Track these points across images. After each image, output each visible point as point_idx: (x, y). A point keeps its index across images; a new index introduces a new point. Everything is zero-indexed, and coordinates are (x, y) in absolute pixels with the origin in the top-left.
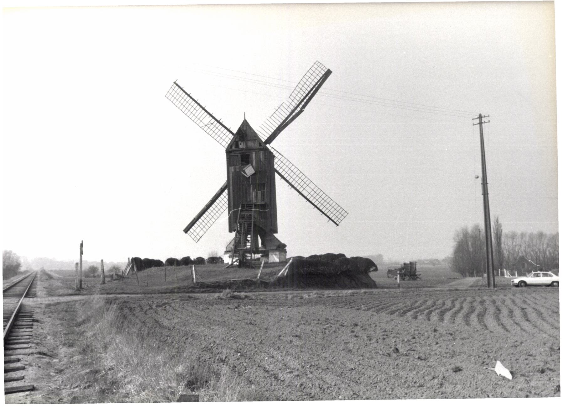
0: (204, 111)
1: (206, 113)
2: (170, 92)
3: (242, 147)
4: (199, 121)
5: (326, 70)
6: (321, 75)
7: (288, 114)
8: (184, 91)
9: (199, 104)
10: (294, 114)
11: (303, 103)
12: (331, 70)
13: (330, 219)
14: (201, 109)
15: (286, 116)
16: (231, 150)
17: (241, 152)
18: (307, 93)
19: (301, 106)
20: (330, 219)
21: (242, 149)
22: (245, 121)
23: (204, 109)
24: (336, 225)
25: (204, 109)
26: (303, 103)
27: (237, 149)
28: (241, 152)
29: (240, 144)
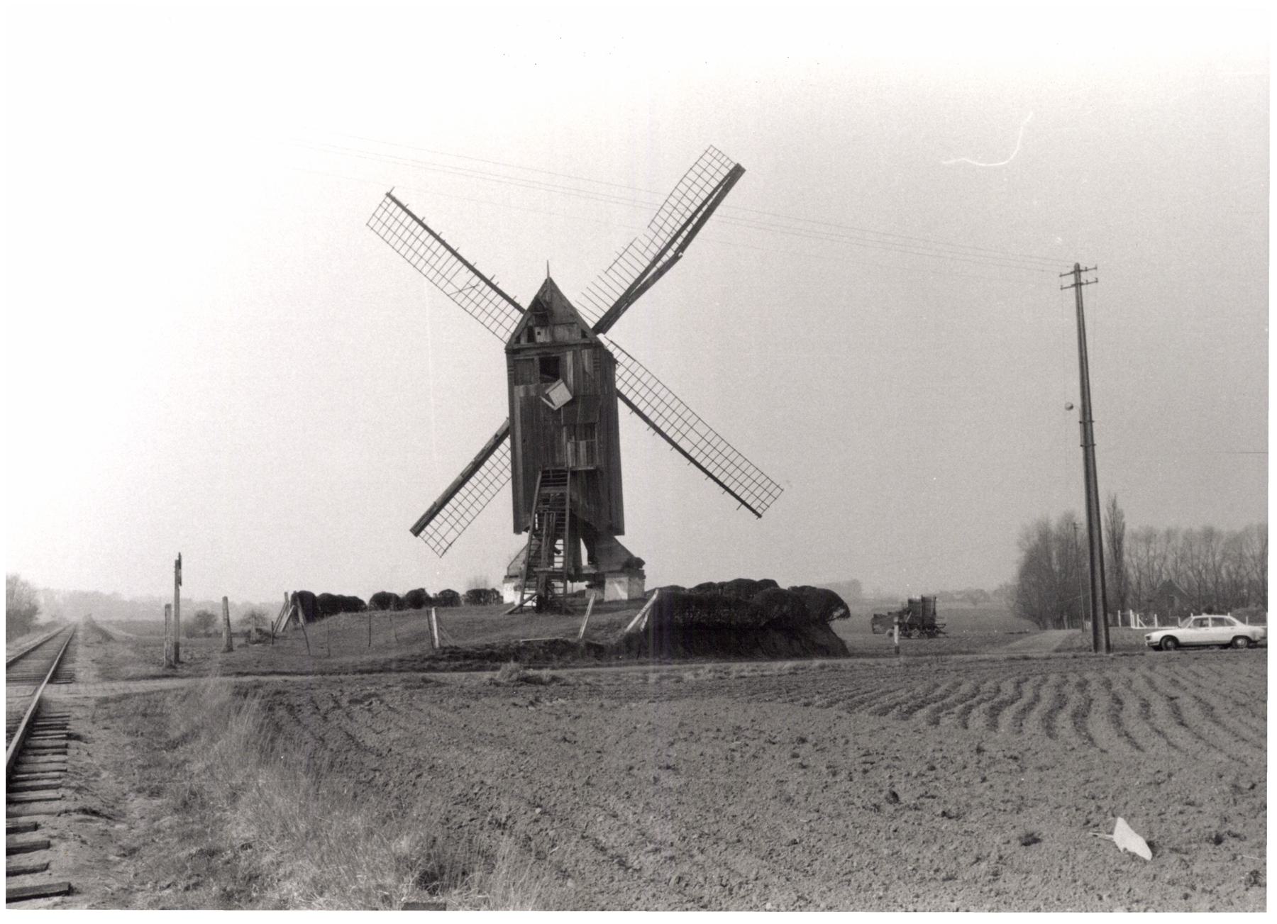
0: (454, 259)
1: (460, 264)
2: (378, 215)
3: (542, 341)
4: (444, 281)
5: (731, 167)
6: (720, 178)
7: (647, 263)
8: (409, 213)
9: (443, 243)
10: (659, 264)
11: (680, 240)
12: (743, 165)
13: (743, 502)
14: (448, 253)
15: (642, 269)
16: (516, 347)
17: (539, 351)
18: (688, 217)
19: (675, 246)
20: (743, 502)
21: (543, 345)
22: (548, 281)
23: (454, 253)
24: (756, 517)
25: (454, 253)
26: (680, 240)
27: (531, 345)
28: (539, 351)
29: (539, 333)
